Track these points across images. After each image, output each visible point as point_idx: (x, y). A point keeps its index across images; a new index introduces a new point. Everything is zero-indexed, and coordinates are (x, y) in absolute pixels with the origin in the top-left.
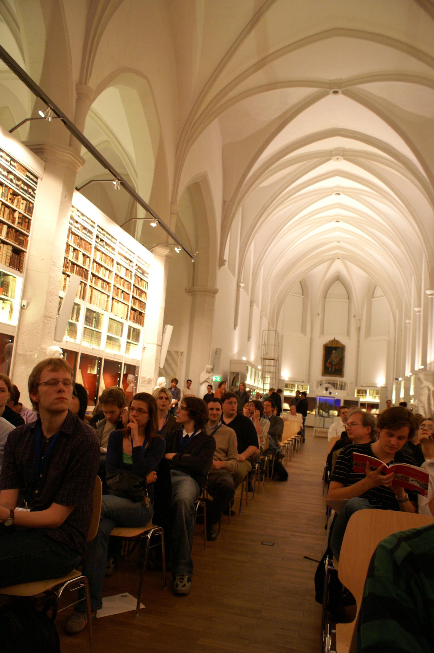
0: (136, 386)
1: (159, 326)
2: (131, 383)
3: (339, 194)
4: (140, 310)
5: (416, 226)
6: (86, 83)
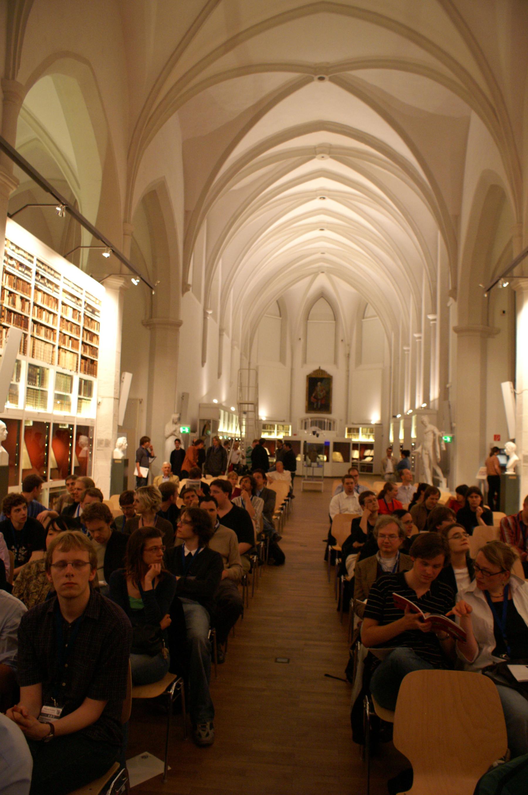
0: (91, 450)
1: (115, 376)
2: (84, 447)
3: (324, 198)
4: (92, 358)
6: (13, 78)
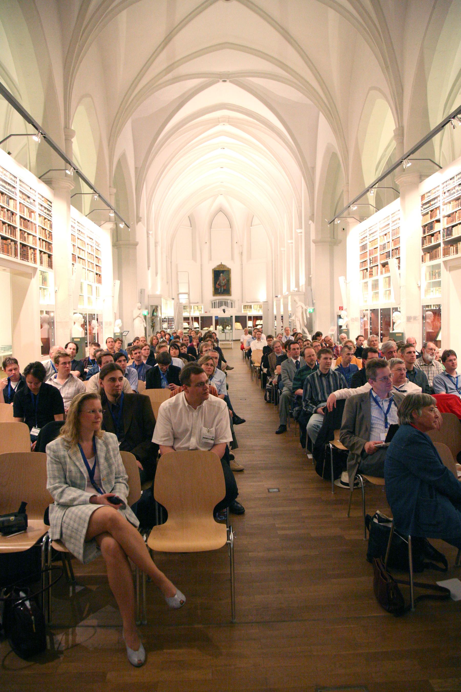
5: (287, 177)
